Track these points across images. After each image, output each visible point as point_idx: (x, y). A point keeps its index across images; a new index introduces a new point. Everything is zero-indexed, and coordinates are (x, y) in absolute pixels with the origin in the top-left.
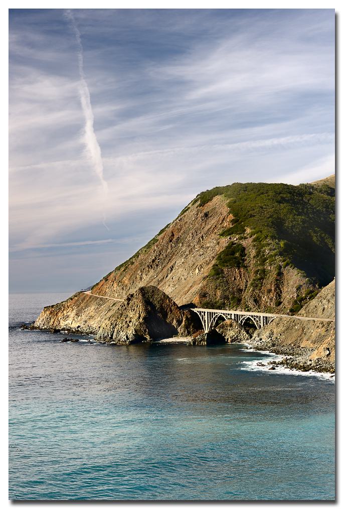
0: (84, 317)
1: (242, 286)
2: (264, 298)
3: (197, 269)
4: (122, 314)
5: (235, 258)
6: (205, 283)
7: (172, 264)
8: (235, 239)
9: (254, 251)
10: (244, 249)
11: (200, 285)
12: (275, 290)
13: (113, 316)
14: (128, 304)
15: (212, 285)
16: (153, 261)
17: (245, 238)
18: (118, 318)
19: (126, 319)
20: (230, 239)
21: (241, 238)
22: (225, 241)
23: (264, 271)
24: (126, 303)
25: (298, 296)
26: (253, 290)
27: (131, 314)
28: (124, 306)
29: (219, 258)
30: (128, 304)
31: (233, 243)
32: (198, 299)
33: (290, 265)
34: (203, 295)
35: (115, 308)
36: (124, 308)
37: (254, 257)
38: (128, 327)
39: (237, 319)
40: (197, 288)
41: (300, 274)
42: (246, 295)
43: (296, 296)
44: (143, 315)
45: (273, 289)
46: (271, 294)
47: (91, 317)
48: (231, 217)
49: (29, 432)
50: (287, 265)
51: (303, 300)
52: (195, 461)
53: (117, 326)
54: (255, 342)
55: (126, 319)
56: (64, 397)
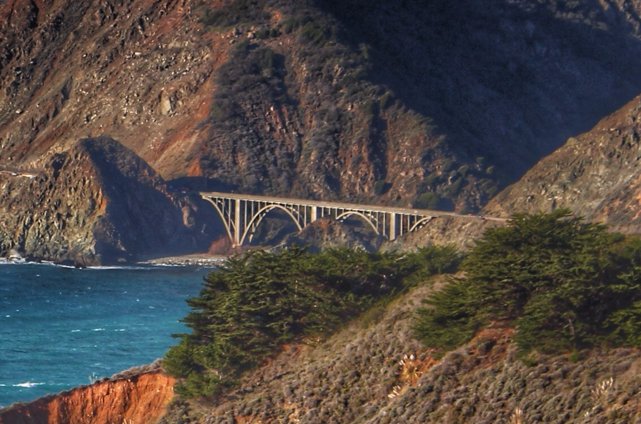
2: (347, 175)
4: (42, 198)
5: (264, 81)
6: (205, 134)
7: (59, 85)
8: (250, 35)
9: (304, 67)
12: (371, 158)
14: (56, 175)
15: (224, 139)
18: (35, 206)
19: (56, 208)
20: (238, 33)
23: (340, 115)
24: (50, 172)
25: (427, 174)
26: (321, 158)
27: (70, 198)
28: (47, 179)
29: (226, 79)
30: (56, 175)
31: (249, 47)
33: (397, 102)
36: (47, 183)
37: (308, 80)
38: (64, 227)
42: (306, 170)
43: (422, 173)
45: (365, 155)
46: (363, 168)
50: (389, 102)
51: (440, 183)
53: (35, 224)
54: (374, 371)
55: (56, 208)
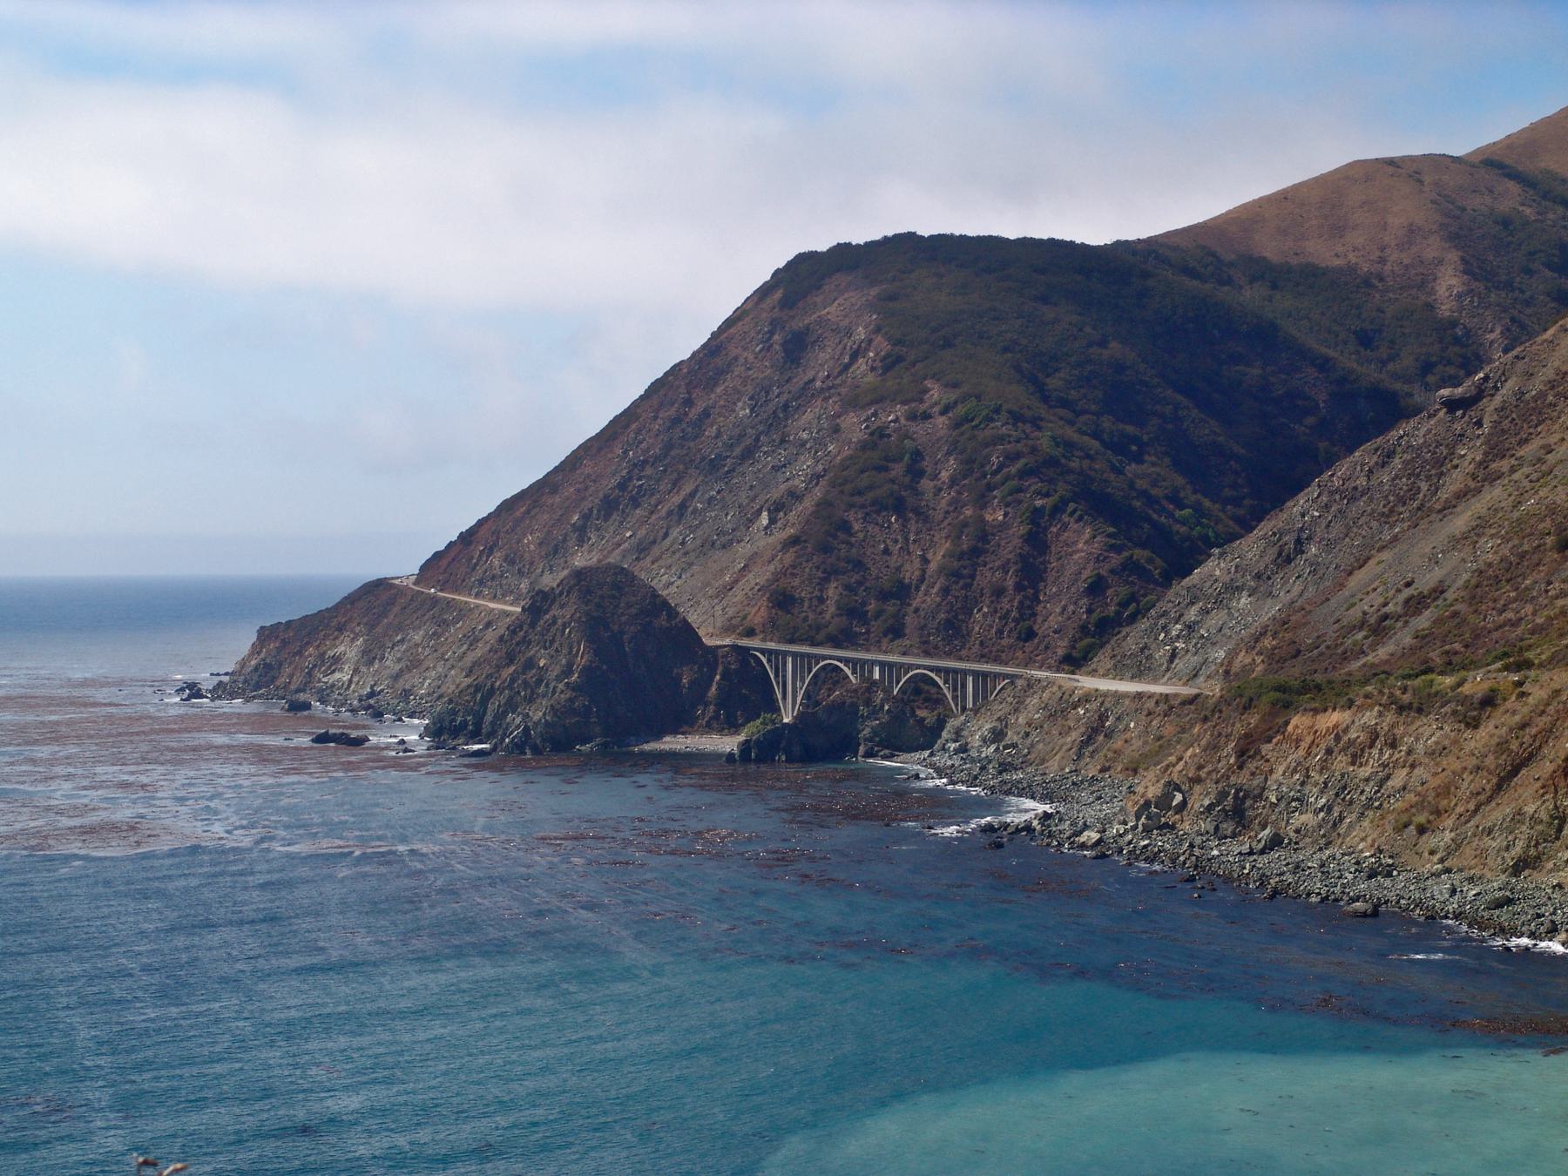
0: (391, 663)
1: (911, 572)
3: (765, 514)
6: (789, 557)
10: (917, 455)
11: (772, 567)
13: (476, 664)
16: (622, 486)
17: (926, 416)
21: (912, 417)
22: (855, 426)
31: (881, 433)
32: (763, 612)
34: (782, 601)
35: (491, 636)
39: (890, 682)
40: (760, 576)
41: (1098, 539)
44: (581, 661)
47: (414, 664)
48: (882, 345)
49: (13, 672)
52: (373, 1068)
56: (81, 1158)
